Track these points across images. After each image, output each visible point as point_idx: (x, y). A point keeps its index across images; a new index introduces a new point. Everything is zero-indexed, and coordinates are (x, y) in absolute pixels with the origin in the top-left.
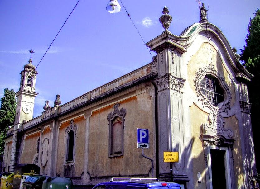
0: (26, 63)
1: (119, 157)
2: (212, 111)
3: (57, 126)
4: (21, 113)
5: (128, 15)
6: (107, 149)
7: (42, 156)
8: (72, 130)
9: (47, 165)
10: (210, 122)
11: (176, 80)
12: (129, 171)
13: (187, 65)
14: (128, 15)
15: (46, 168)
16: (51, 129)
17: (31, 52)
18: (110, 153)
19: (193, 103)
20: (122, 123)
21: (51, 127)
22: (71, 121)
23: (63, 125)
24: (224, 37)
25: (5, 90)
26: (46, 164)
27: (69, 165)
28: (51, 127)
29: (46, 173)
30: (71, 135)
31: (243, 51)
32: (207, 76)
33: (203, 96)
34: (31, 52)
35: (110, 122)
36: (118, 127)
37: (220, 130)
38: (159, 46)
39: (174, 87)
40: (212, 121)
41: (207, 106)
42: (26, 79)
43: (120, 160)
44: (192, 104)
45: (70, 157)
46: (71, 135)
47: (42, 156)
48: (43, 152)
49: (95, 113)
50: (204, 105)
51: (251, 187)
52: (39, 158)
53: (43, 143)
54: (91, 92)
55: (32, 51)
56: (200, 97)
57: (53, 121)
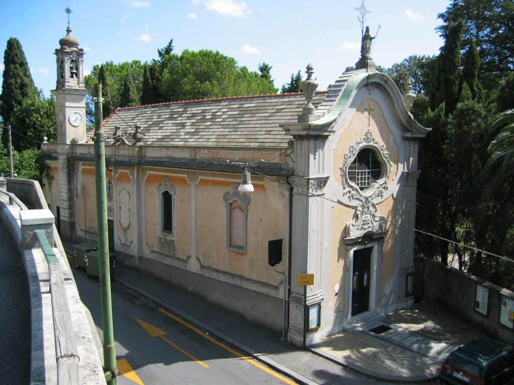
0: (63, 35)
1: (242, 254)
2: (360, 203)
3: (141, 175)
4: (69, 128)
6: (225, 238)
7: (120, 212)
8: (167, 191)
9: (131, 227)
15: (128, 231)
16: (132, 178)
17: (68, 11)
18: (228, 245)
20: (245, 210)
22: (167, 176)
23: (150, 176)
25: (439, 17)
26: (129, 228)
28: (133, 174)
29: (130, 240)
30: (167, 199)
31: (367, 59)
34: (68, 11)
35: (228, 204)
36: (238, 215)
38: (192, 330)
42: (67, 65)
43: (242, 257)
45: (167, 225)
46: (167, 199)
47: (120, 212)
48: (120, 207)
49: (202, 182)
52: (119, 210)
53: (119, 194)
54: (46, 255)
55: (69, 10)
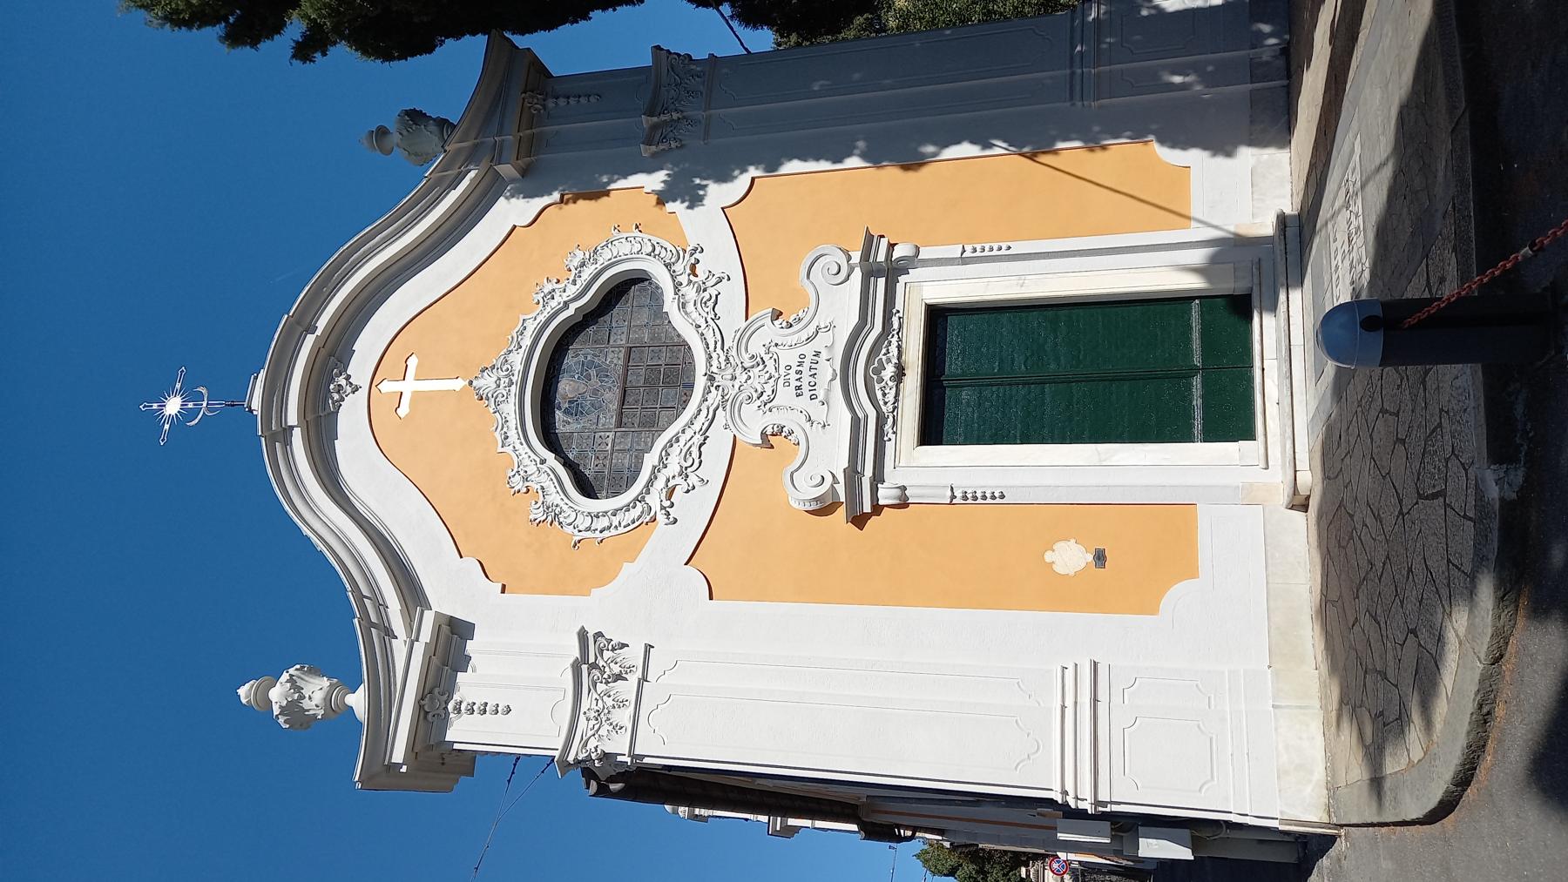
11: (585, 704)
33: (650, 483)
37: (817, 354)
39: (624, 717)
40: (770, 420)
41: (695, 454)
50: (693, 479)
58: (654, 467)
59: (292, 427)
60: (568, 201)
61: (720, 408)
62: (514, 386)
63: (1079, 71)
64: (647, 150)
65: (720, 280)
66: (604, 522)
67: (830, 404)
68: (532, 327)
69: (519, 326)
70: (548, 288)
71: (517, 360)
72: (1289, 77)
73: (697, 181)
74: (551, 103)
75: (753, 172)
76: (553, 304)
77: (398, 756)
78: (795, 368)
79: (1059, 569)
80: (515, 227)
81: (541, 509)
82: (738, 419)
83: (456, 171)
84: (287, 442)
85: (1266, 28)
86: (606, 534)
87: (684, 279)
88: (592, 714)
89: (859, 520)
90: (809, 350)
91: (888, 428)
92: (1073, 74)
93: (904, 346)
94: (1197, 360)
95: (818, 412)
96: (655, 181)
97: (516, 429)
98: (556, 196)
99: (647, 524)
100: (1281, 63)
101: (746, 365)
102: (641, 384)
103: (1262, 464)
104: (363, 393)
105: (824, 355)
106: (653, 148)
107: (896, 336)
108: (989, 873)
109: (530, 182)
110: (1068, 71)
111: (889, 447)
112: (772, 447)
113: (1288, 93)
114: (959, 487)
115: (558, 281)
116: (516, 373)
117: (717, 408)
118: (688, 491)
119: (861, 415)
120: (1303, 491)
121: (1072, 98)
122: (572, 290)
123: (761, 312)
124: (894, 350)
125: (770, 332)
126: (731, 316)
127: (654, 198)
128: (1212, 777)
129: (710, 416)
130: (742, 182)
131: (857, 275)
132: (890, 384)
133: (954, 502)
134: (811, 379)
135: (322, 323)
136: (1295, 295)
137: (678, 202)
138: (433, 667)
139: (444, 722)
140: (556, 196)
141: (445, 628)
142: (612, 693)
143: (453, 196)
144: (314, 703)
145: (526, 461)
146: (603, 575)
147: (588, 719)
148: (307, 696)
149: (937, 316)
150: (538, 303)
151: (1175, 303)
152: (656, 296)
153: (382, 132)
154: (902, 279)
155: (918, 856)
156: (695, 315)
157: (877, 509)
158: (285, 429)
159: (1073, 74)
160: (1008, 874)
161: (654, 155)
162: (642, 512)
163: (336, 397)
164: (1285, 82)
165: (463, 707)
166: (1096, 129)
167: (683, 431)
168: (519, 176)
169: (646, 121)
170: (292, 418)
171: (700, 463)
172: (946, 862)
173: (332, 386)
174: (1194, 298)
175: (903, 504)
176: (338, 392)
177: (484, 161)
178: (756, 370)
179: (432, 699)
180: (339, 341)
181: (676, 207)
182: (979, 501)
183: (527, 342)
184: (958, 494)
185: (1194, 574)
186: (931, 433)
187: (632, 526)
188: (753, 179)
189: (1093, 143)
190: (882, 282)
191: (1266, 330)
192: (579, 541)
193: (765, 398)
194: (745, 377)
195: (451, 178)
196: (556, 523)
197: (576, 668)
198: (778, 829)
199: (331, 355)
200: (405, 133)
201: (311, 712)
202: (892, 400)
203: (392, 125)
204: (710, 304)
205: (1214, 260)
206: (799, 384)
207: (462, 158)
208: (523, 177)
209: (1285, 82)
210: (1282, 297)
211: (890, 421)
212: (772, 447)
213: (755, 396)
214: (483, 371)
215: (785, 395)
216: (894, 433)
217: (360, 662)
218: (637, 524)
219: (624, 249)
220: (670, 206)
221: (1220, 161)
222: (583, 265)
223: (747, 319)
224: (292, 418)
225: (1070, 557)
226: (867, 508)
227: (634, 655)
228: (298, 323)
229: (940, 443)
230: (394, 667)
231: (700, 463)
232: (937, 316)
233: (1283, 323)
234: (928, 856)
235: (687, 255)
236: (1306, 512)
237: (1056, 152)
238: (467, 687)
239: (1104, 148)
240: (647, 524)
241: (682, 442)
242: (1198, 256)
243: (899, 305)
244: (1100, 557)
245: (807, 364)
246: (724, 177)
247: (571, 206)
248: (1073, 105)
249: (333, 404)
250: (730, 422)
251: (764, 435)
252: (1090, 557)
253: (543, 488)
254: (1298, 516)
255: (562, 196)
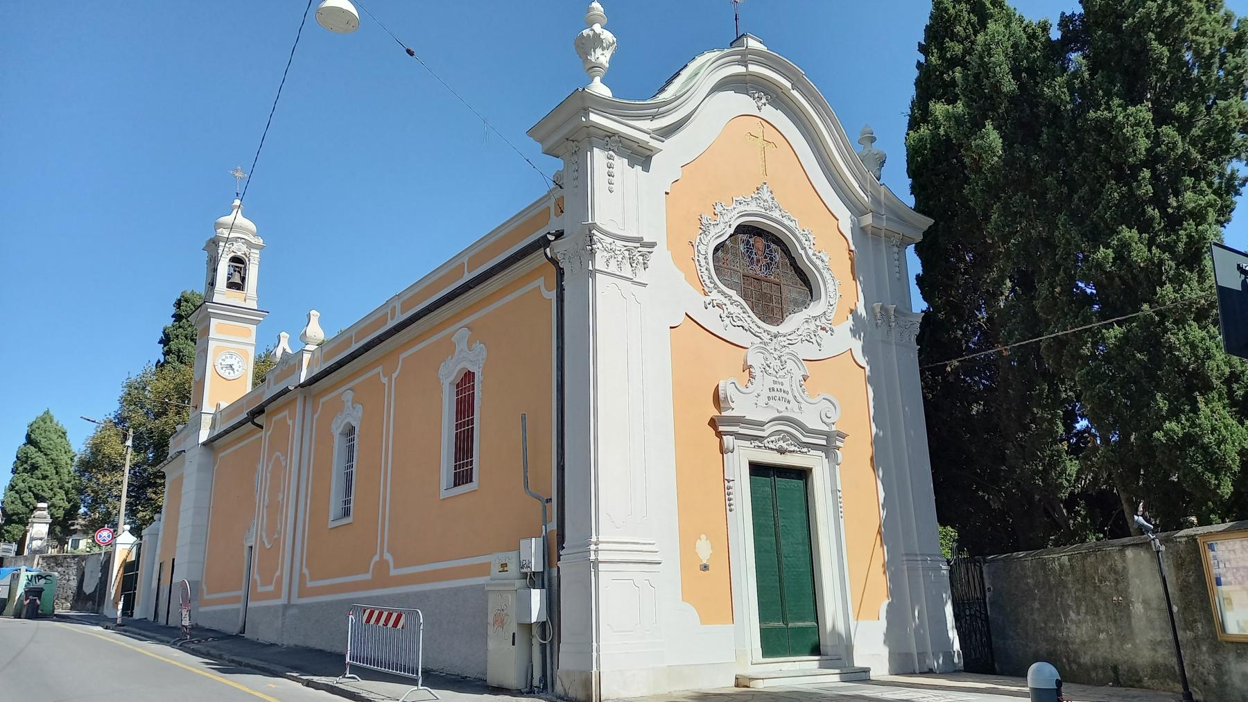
3: (308, 412)
5: (410, 53)
10: (751, 376)
11: (619, 243)
12: (802, 570)
13: (667, 193)
14: (410, 53)
19: (686, 314)
21: (293, 417)
24: (598, 114)
27: (1083, 593)
32: (741, 229)
33: (723, 293)
37: (789, 402)
39: (613, 268)
40: (757, 371)
41: (740, 323)
42: (223, 268)
44: (680, 319)
50: (727, 321)
51: (281, 528)
56: (715, 295)
57: (296, 398)
58: (731, 297)
59: (746, 67)
60: (850, 254)
61: (761, 341)
62: (764, 211)
63: (919, 559)
64: (877, 306)
65: (819, 345)
66: (703, 263)
67: (767, 409)
68: (792, 224)
69: (792, 218)
70: (811, 239)
71: (776, 214)
72: (920, 673)
73: (862, 335)
74: (896, 249)
75: (868, 368)
76: (804, 241)
77: (594, 117)
78: (783, 388)
79: (699, 543)
80: (838, 220)
81: (707, 223)
82: (793, 358)
83: (869, 189)
84: (740, 63)
85: (941, 661)
86: (697, 264)
87: (818, 323)
88: (613, 246)
89: (713, 423)
90: (790, 397)
91: (757, 443)
92: (916, 555)
93: (794, 454)
94: (790, 625)
95: (762, 401)
96: (862, 311)
97: (745, 211)
98: (853, 248)
99: (703, 290)
100: (926, 670)
101: (782, 358)
102: (764, 291)
103: (754, 662)
104: (757, 113)
105: (788, 405)
106: (878, 310)
107: (798, 450)
108: (32, 474)
109: (860, 232)
110: (918, 553)
111: (747, 443)
112: (744, 371)
113: (911, 673)
114: (734, 484)
115: (814, 244)
116: (770, 213)
117: (761, 338)
118: (721, 317)
119: (765, 427)
120: (752, 684)
121: (906, 554)
122: (810, 252)
123: (808, 368)
124: (792, 448)
125: (798, 375)
126: (805, 351)
127: (853, 308)
128: (615, 632)
129: (757, 334)
130: (863, 362)
131: (826, 429)
132: (778, 445)
133: (726, 482)
134: (778, 398)
135: (795, 93)
136: (837, 678)
137: (853, 323)
138: (645, 151)
139: (604, 148)
140: (853, 248)
141: (649, 153)
142: (624, 260)
143: (856, 185)
144: (600, 56)
145: (729, 216)
146: (677, 259)
147: (611, 244)
148: (604, 52)
149: (803, 474)
150: (804, 231)
151: (815, 612)
152: (805, 305)
153: (873, 140)
154: (823, 454)
155: (47, 413)
156: (802, 328)
157: (719, 435)
158: (746, 62)
159: (916, 555)
160: (30, 491)
161: (873, 309)
162: (709, 287)
163: (756, 95)
164: (917, 671)
165: (611, 161)
166: (893, 569)
167: (749, 316)
168: (862, 226)
169: (892, 307)
170: (753, 68)
171: (735, 326)
172: (43, 437)
173: (763, 94)
174: (818, 623)
175: (723, 451)
176: (758, 97)
177: (872, 206)
178: (779, 364)
179: (616, 141)
180: (787, 106)
181: (850, 322)
182: (727, 497)
183: (787, 222)
184: (731, 484)
185: (703, 622)
186: (757, 469)
187: (701, 280)
188: (863, 368)
189: (887, 566)
190: (824, 442)
191: (810, 663)
192: (693, 245)
193: (767, 368)
194: (776, 357)
195: (865, 185)
196: (701, 231)
197: (639, 240)
198: (209, 310)
199: (778, 96)
200: (877, 156)
201: (593, 53)
202: (770, 446)
203: (876, 147)
204: (808, 338)
205: (839, 635)
206: (775, 389)
207: (875, 194)
208: (861, 228)
209: (917, 671)
210: (837, 671)
211: (760, 445)
212: (744, 371)
213: (768, 362)
214: (771, 192)
215: (769, 381)
216: (754, 447)
217: (635, 100)
218: (703, 283)
219: (831, 287)
220: (850, 317)
221: (882, 638)
222: (823, 261)
223: (804, 360)
224: (753, 68)
225: (704, 550)
226: (721, 429)
227: (642, 276)
228: (798, 80)
229: (751, 475)
230: (633, 120)
231: (735, 326)
232: (803, 474)
233: (814, 672)
234: (48, 422)
235: (829, 325)
236: (735, 686)
237: (882, 545)
238: (620, 163)
239: (884, 573)
240: (703, 290)
241: (742, 314)
242: (841, 628)
243: (812, 452)
244: (705, 568)
245: (785, 395)
246: (866, 351)
247: (848, 256)
248: (902, 555)
249: (753, 93)
250: (755, 346)
251: (751, 366)
252: (705, 562)
253: (1217, 366)
254: (733, 683)
255: (852, 251)
